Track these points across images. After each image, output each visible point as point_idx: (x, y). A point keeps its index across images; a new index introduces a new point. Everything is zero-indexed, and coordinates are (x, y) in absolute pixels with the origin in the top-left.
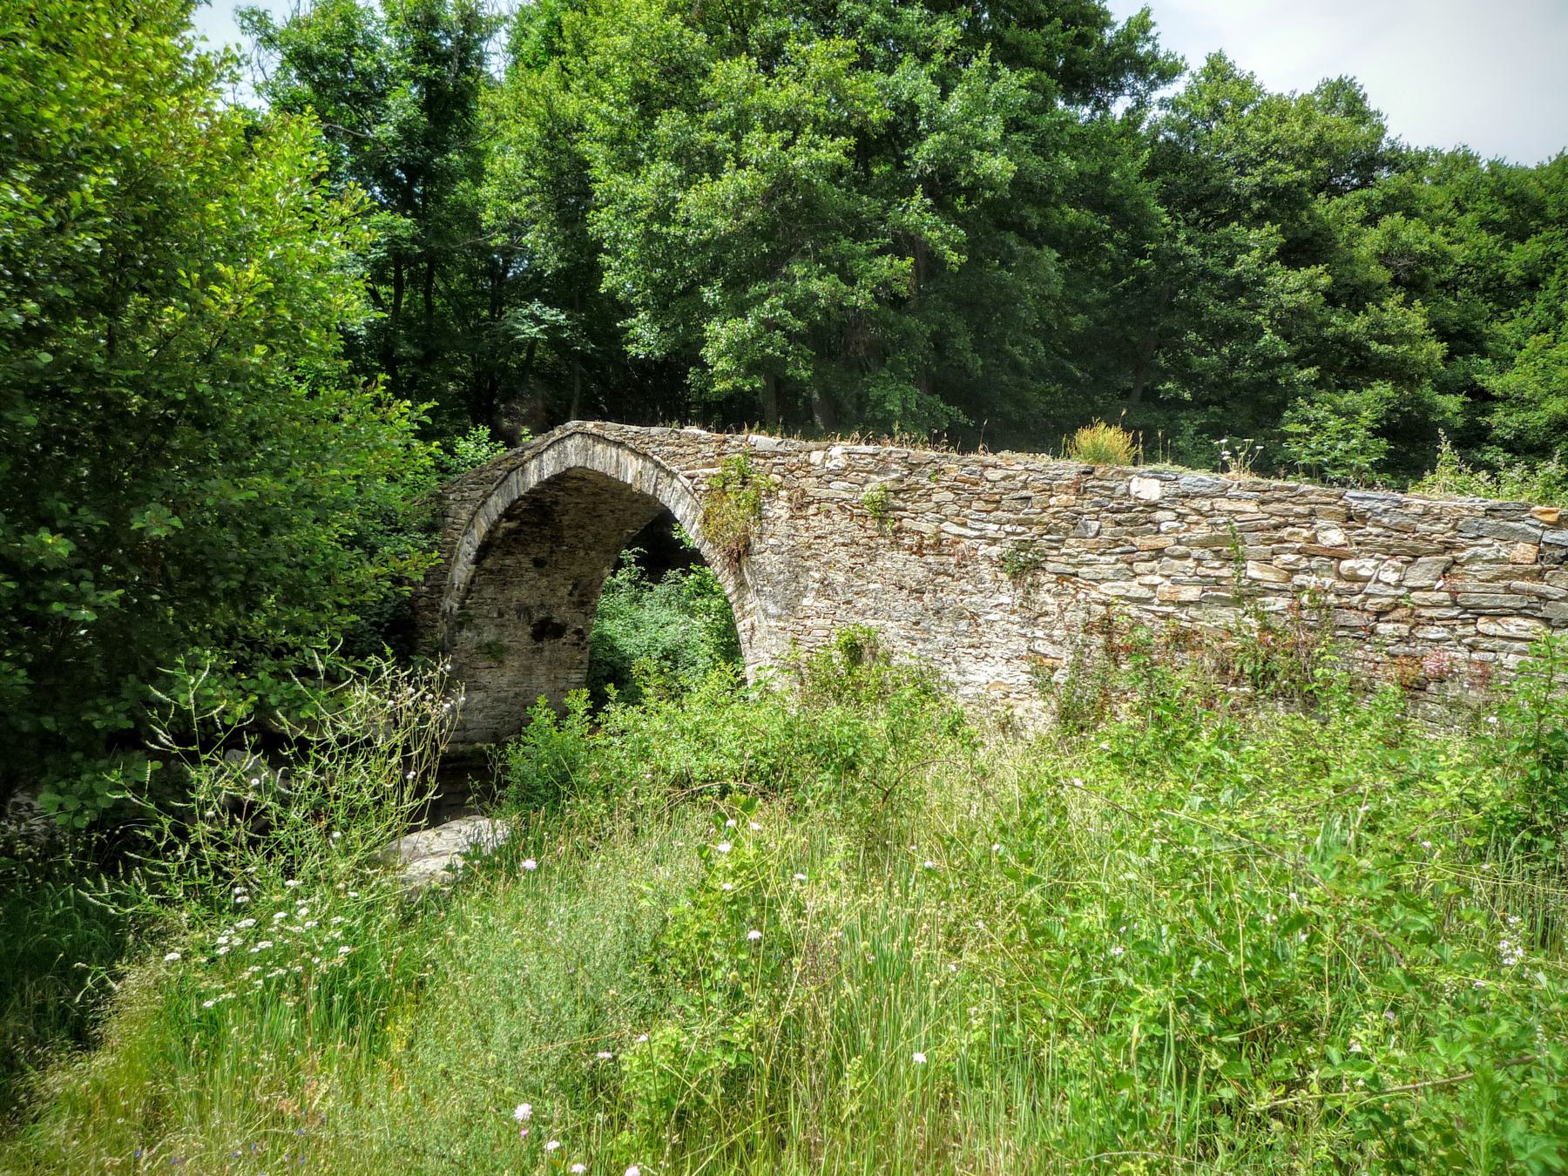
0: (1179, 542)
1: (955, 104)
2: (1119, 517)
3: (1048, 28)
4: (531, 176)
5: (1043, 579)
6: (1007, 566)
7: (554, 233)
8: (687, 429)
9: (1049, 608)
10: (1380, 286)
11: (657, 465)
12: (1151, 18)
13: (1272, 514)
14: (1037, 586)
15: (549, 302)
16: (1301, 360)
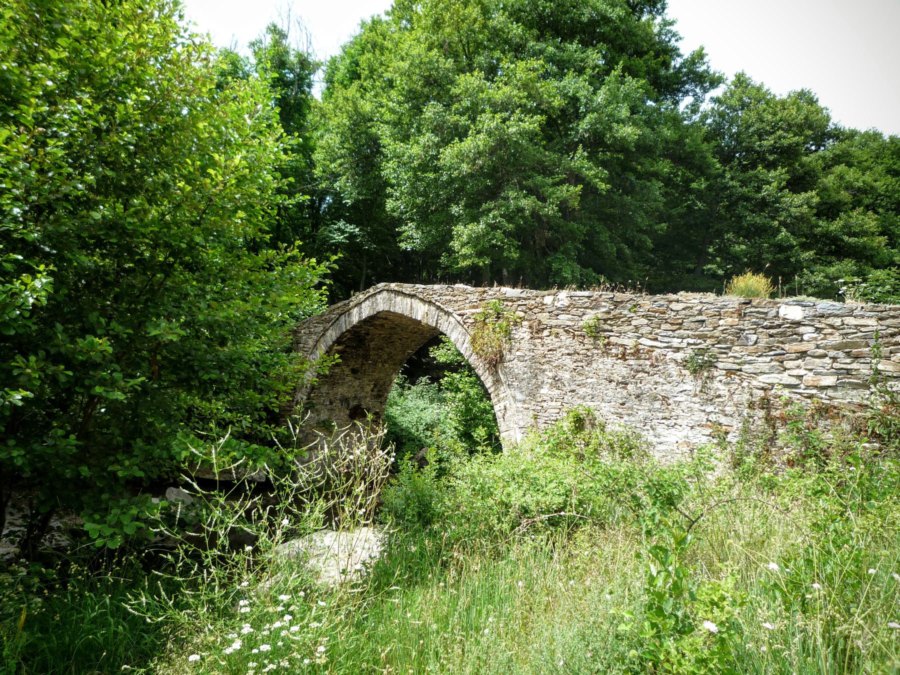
0: (818, 347)
1: (600, 97)
2: (772, 331)
3: (646, 57)
4: (344, 148)
5: (716, 374)
6: (689, 365)
7: (355, 180)
8: (457, 285)
9: (721, 393)
10: (846, 204)
11: (438, 308)
12: (704, 52)
13: (888, 327)
14: (711, 378)
15: (349, 221)
16: (805, 247)
